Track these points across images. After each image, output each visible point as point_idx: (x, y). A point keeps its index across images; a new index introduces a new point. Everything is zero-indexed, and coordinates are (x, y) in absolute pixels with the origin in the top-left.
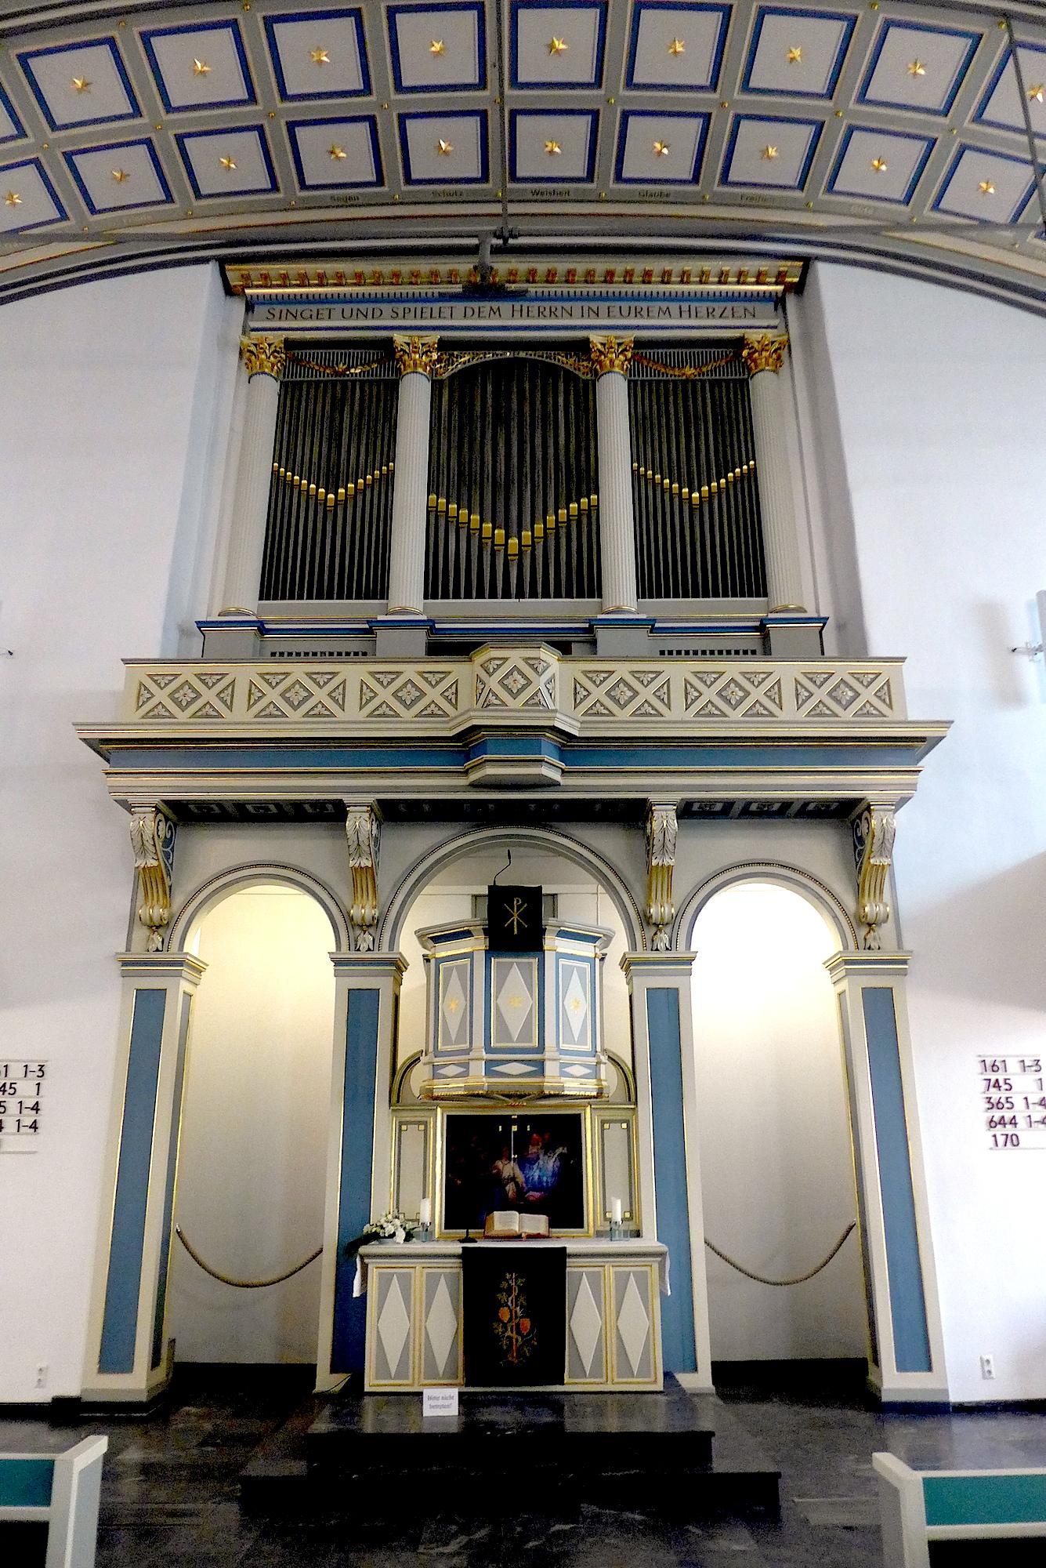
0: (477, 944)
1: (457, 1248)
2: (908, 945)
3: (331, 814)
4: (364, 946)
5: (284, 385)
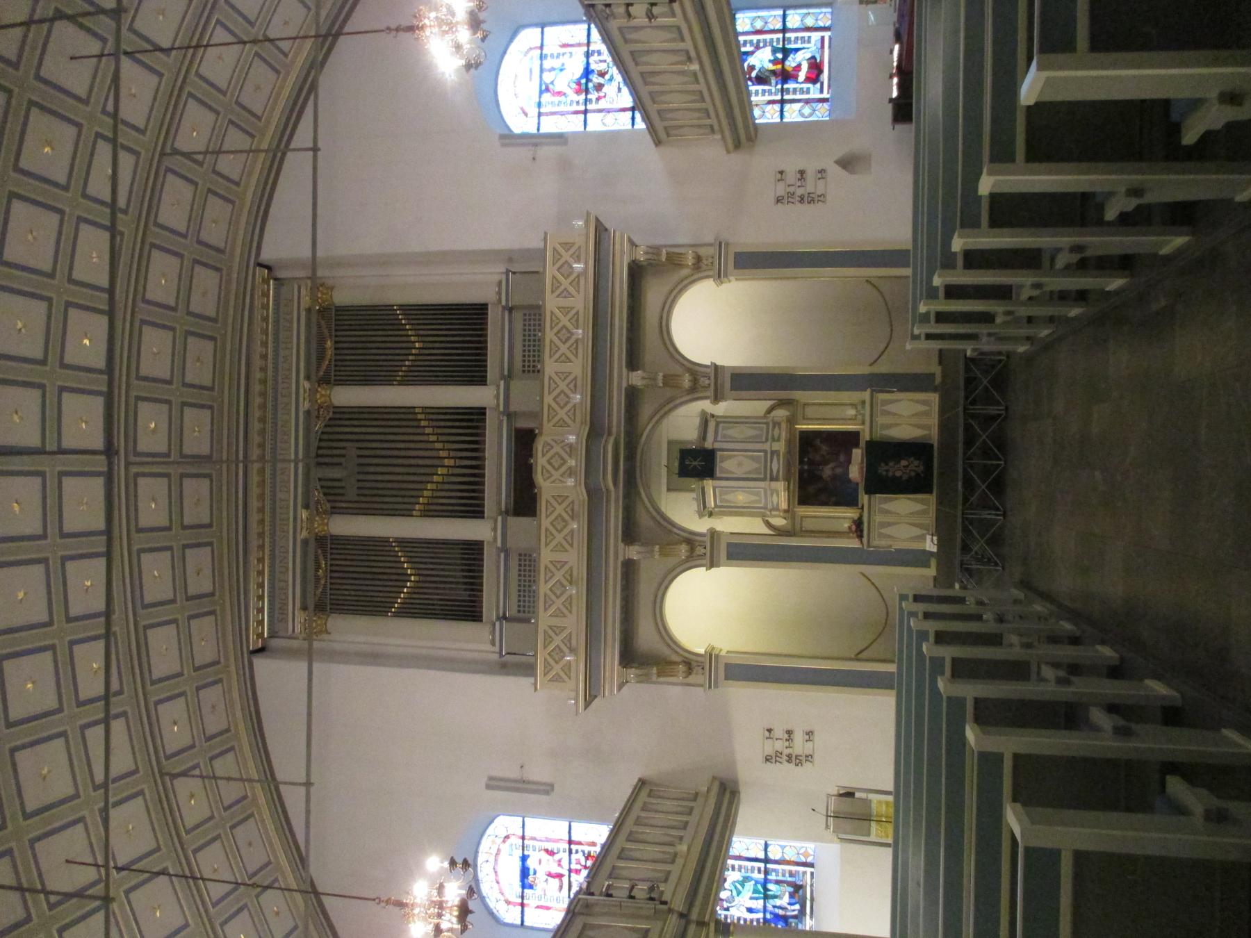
0: (709, 484)
1: (866, 497)
2: (712, 241)
3: (629, 568)
4: (703, 551)
5: (333, 611)
